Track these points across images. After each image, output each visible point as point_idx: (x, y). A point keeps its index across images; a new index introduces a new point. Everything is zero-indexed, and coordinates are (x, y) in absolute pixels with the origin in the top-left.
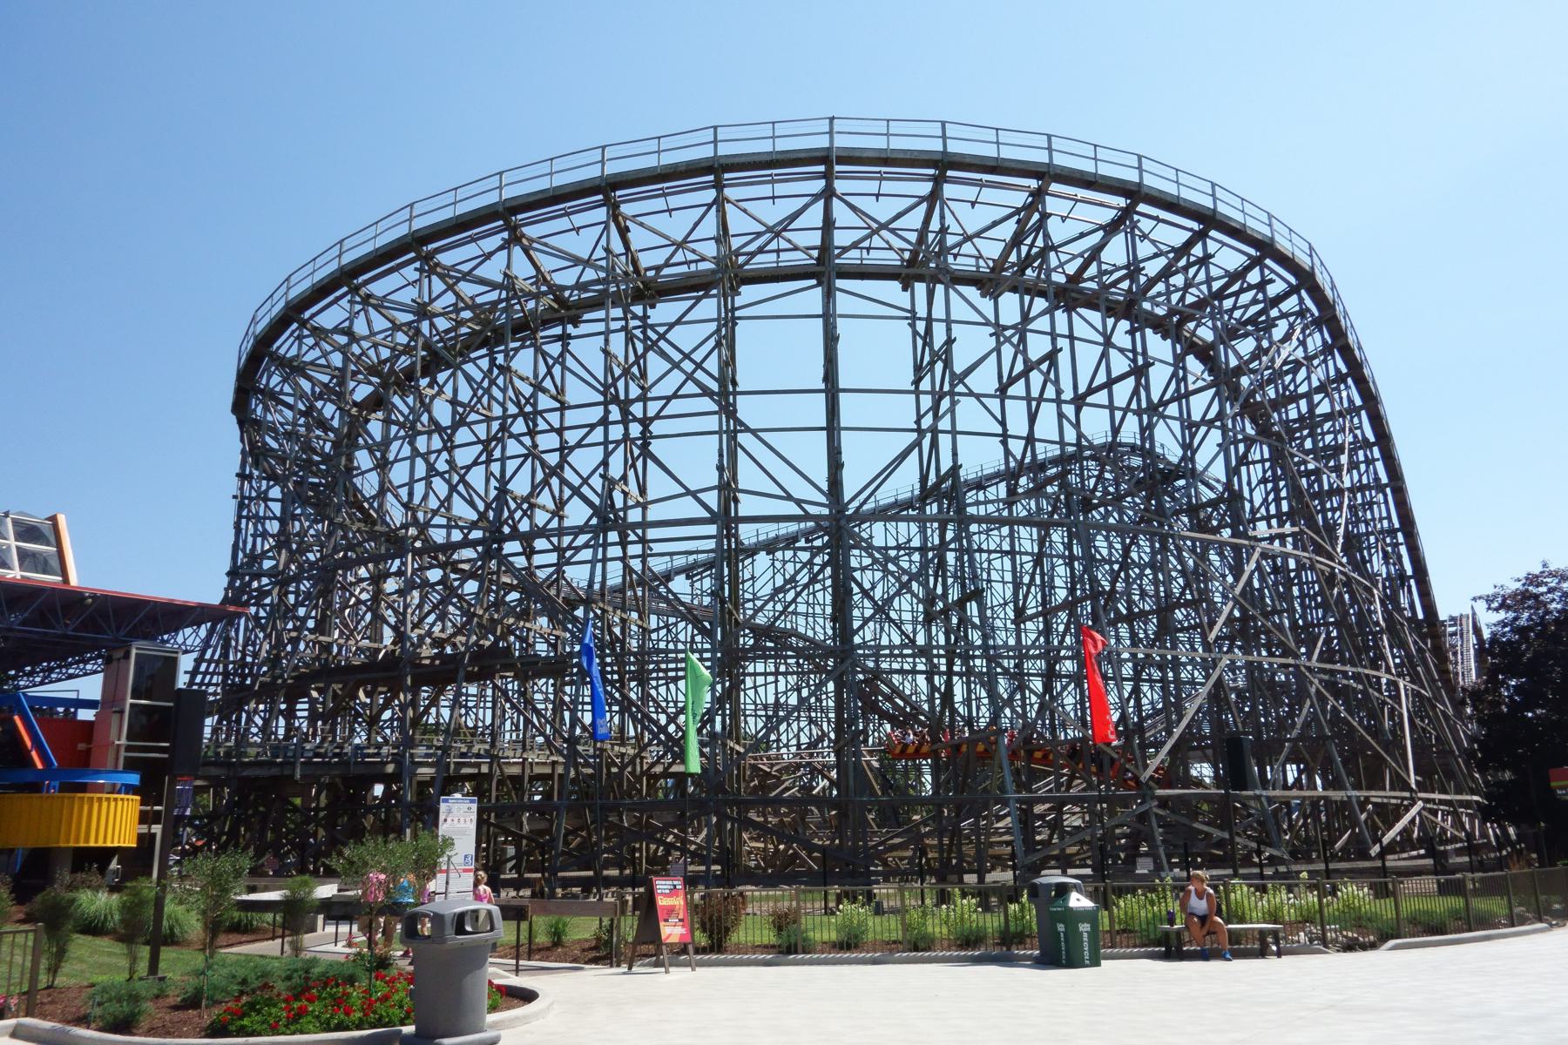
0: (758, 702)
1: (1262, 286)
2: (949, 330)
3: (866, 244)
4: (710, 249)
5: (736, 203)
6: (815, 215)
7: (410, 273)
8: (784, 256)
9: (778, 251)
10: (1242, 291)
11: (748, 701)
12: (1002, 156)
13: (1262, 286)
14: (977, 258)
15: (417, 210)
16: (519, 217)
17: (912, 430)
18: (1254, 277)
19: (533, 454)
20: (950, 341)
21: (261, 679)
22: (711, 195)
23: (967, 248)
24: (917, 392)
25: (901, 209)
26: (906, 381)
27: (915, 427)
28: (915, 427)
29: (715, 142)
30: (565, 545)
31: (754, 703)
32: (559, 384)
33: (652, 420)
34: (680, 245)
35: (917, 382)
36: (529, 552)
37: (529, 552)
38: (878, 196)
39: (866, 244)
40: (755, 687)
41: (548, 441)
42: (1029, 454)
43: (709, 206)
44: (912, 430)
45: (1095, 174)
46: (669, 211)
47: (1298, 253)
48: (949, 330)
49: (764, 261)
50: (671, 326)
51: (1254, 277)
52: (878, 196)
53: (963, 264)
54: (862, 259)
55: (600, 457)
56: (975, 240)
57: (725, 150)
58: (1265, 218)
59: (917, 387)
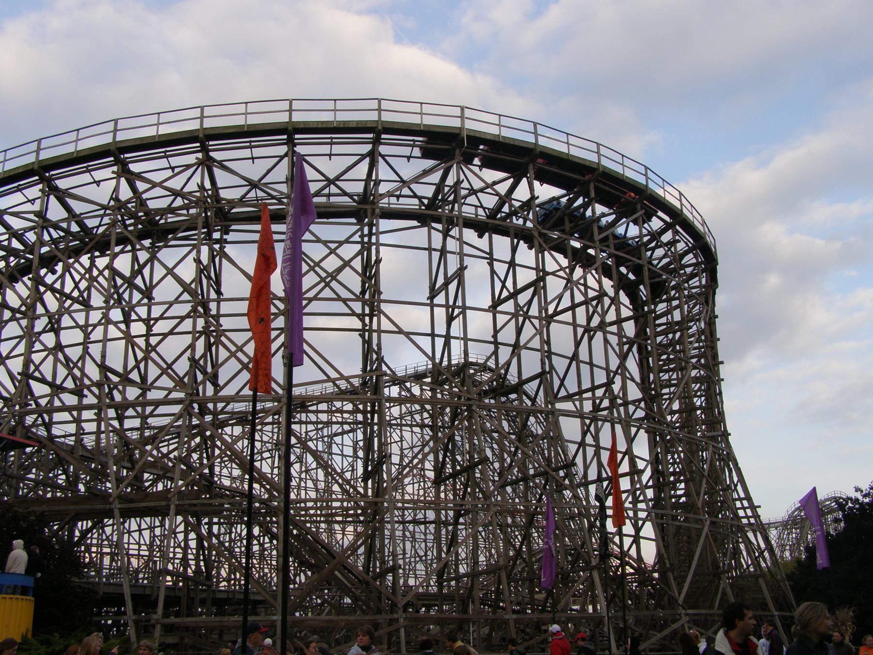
0: (142, 542)
1: (673, 243)
2: (462, 260)
3: (326, 191)
4: (359, 188)
5: (383, 157)
6: (363, 169)
7: (34, 192)
8: (333, 199)
9: (329, 195)
10: (657, 247)
11: (132, 541)
12: (503, 134)
13: (673, 243)
14: (476, 207)
15: (44, 144)
16: (126, 155)
17: (491, 342)
18: (667, 237)
19: (129, 338)
20: (462, 268)
21: (847, 640)
22: (283, 149)
23: (472, 200)
24: (432, 306)
25: (270, 167)
26: (424, 298)
27: (492, 340)
28: (492, 340)
29: (290, 111)
30: (147, 412)
31: (139, 544)
32: (557, 301)
33: (188, 316)
34: (330, 182)
35: (432, 297)
36: (121, 418)
37: (121, 418)
38: (330, 155)
39: (326, 191)
40: (140, 530)
41: (138, 328)
42: (445, 359)
43: (282, 158)
44: (491, 342)
45: (568, 154)
46: (253, 158)
47: (696, 223)
48: (462, 260)
49: (393, 203)
50: (341, 243)
51: (667, 237)
52: (330, 155)
53: (468, 211)
54: (389, 204)
55: (190, 341)
56: (479, 194)
57: (297, 117)
58: (677, 195)
59: (432, 301)
